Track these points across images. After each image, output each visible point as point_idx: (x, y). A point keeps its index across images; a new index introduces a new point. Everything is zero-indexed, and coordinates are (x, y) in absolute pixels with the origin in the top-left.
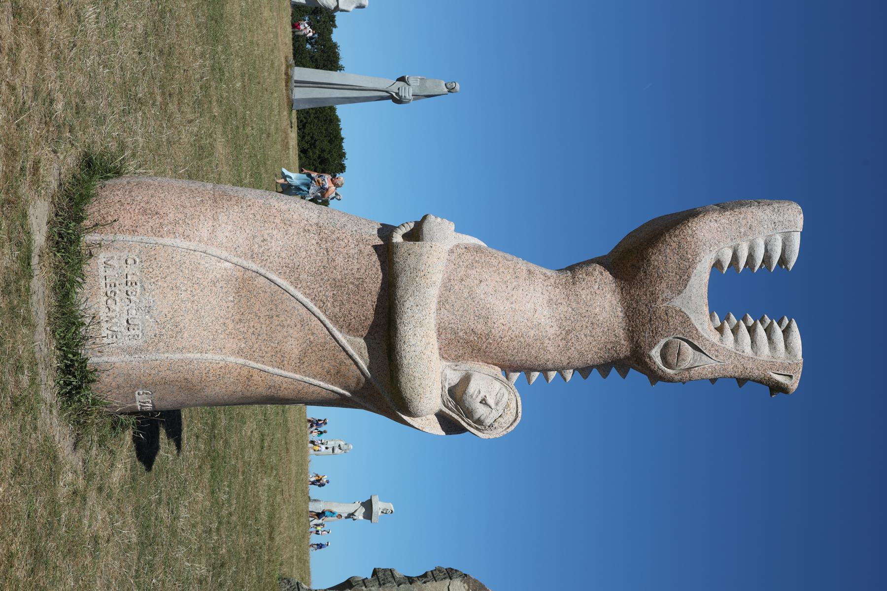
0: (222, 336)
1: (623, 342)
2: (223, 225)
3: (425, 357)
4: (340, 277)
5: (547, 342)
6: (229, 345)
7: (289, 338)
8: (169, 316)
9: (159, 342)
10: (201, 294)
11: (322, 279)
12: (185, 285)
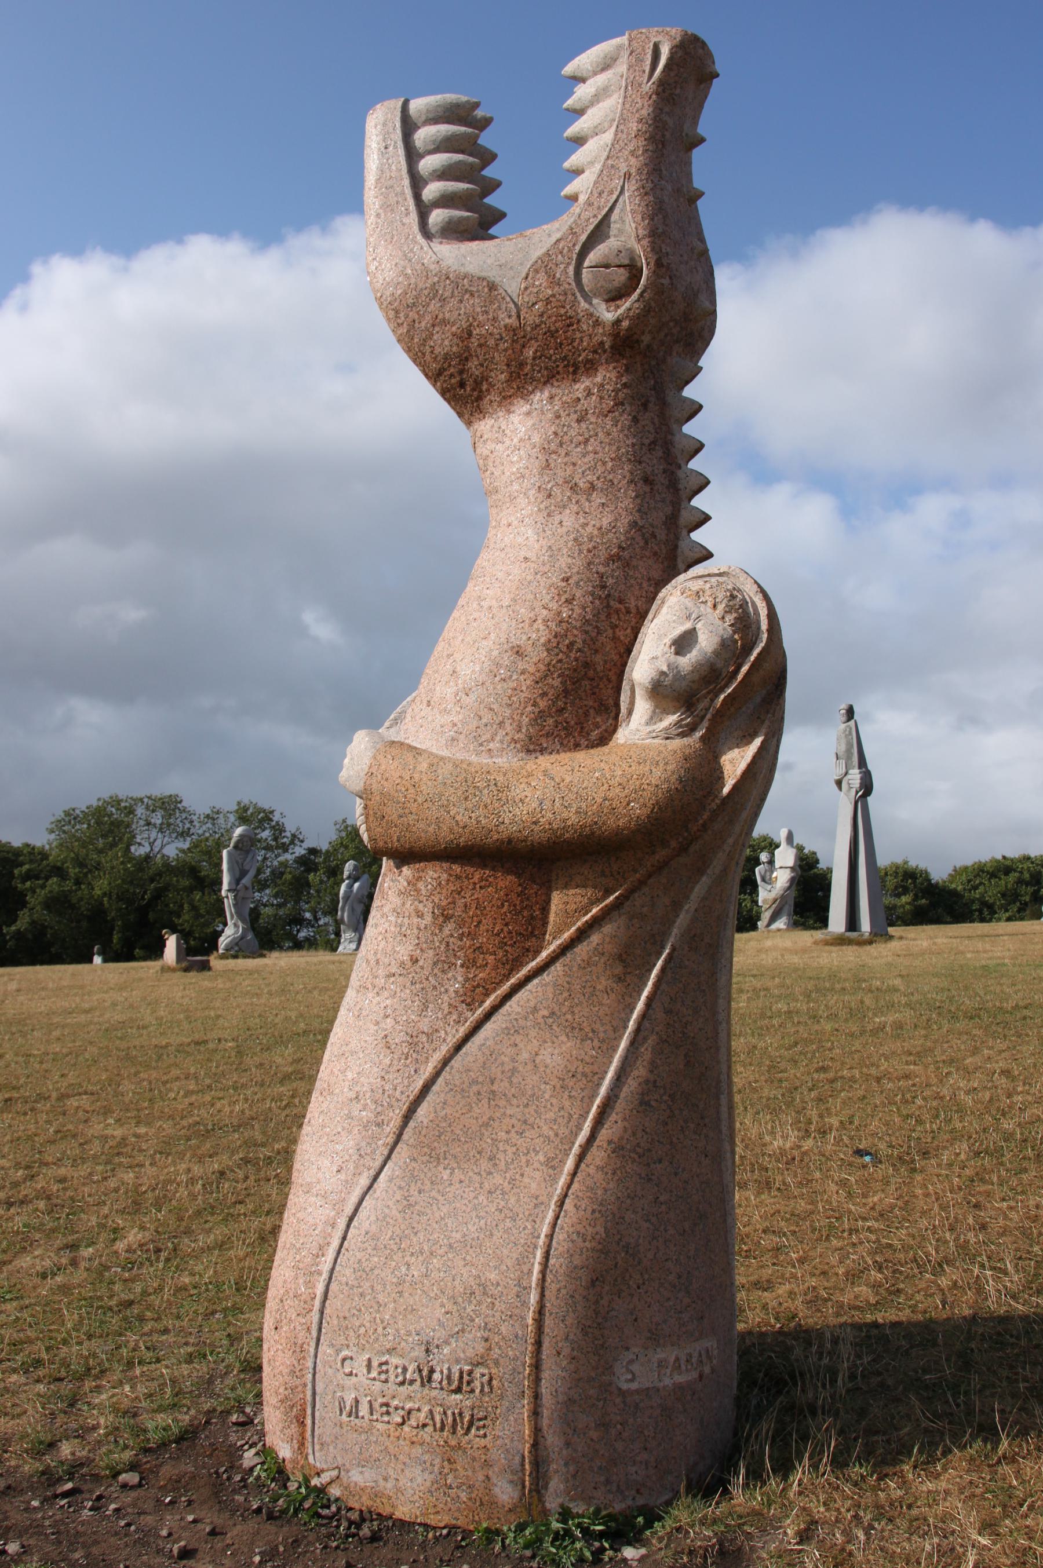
0: (513, 1200)
1: (599, 379)
2: (320, 1175)
3: (568, 779)
4: (431, 953)
5: (589, 529)
6: (534, 1185)
7: (538, 1059)
8: (449, 1306)
9: (499, 1333)
10: (421, 1235)
11: (435, 988)
12: (397, 1267)
